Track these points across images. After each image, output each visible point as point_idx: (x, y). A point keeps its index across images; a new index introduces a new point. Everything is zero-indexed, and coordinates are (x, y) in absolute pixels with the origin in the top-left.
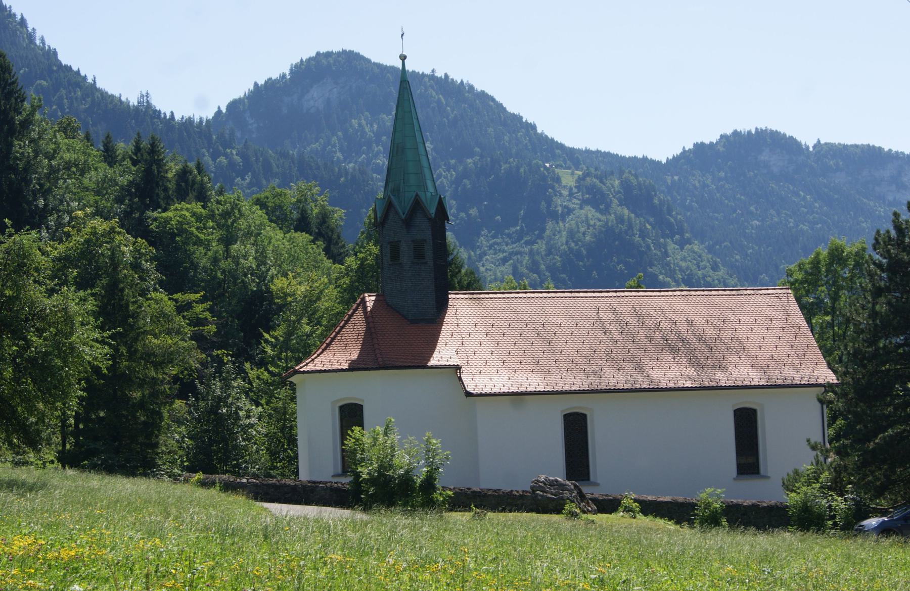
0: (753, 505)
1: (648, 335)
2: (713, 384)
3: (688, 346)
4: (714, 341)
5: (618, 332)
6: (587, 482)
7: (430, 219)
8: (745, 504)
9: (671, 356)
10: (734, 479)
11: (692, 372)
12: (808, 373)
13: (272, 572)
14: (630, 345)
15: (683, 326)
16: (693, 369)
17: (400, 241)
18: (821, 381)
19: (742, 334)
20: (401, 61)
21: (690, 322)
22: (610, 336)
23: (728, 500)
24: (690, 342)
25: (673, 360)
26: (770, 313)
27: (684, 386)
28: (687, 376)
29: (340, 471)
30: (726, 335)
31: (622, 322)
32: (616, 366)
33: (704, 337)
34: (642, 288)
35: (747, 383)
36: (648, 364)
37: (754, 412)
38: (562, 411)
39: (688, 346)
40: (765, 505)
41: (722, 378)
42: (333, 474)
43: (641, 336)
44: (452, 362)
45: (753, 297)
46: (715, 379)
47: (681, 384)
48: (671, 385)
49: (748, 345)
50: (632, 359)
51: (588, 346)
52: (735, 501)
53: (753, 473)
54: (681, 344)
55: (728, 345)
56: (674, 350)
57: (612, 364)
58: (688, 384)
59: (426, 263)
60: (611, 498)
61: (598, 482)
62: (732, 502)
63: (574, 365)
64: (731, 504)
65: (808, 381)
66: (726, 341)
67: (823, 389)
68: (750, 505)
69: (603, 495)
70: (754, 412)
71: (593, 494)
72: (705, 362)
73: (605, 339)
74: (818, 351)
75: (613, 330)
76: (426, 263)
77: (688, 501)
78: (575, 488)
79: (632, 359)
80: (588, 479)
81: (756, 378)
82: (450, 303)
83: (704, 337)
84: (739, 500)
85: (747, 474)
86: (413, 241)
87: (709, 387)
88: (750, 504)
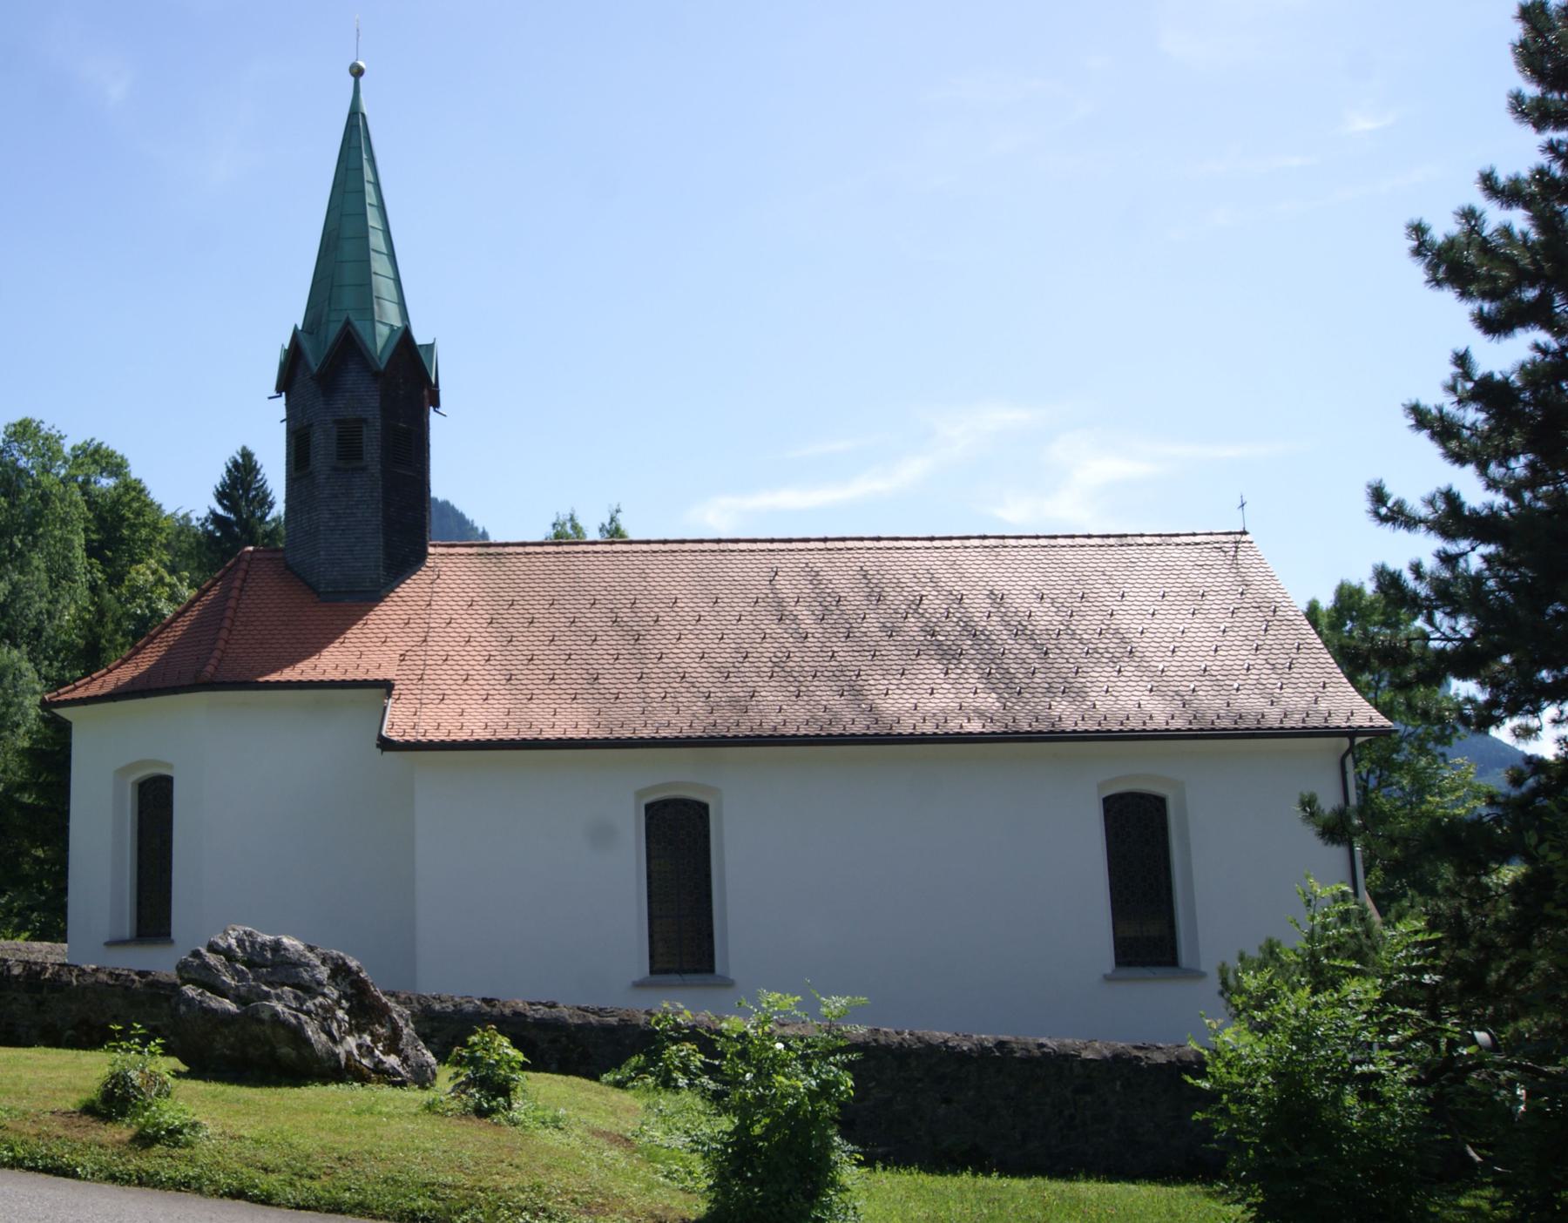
0: (1117, 1058)
1: (889, 625)
2: (1044, 727)
3: (986, 647)
4: (1054, 636)
5: (814, 617)
6: (707, 977)
7: (377, 375)
8: (1088, 1055)
9: (940, 666)
10: (1107, 978)
11: (990, 702)
12: (1302, 704)
13: (355, 1141)
14: (839, 646)
15: (978, 606)
16: (994, 695)
17: (311, 425)
18: (1338, 721)
19: (1123, 621)
20: (352, 79)
21: (997, 599)
22: (794, 626)
23: (1030, 1040)
24: (994, 637)
25: (942, 676)
26: (1198, 579)
27: (962, 731)
28: (976, 710)
29: (127, 928)
30: (1087, 624)
31: (829, 599)
32: (792, 689)
33: (1030, 627)
34: (1367, 872)
35: (1135, 724)
36: (875, 684)
37: (1159, 803)
38: (639, 794)
39: (986, 647)
40: (1160, 1058)
41: (1066, 713)
42: (107, 939)
43: (872, 625)
44: (379, 675)
45: (1159, 550)
46: (1049, 717)
47: (953, 727)
48: (929, 728)
49: (1141, 644)
50: (837, 673)
51: (733, 646)
52: (1052, 1043)
53: (1159, 964)
54: (970, 642)
55: (1091, 646)
56: (949, 656)
57: (785, 684)
58: (975, 727)
59: (364, 469)
60: (613, 1021)
61: (732, 976)
62: (1041, 1046)
63: (685, 685)
64: (1037, 1053)
65: (1304, 721)
66: (1085, 636)
67: (1345, 742)
68: (1105, 1059)
69: (586, 1010)
70: (1159, 803)
71: (553, 1005)
72: (1027, 681)
73: (779, 631)
74: (1327, 658)
75: (802, 612)
76: (364, 469)
77: (882, 1039)
78: (333, 976)
79: (837, 673)
80: (711, 970)
81: (1160, 713)
82: (429, 562)
83: (1030, 627)
84: (1068, 1041)
85: (1144, 964)
86: (336, 422)
87: (1028, 732)
88: (1107, 1053)
